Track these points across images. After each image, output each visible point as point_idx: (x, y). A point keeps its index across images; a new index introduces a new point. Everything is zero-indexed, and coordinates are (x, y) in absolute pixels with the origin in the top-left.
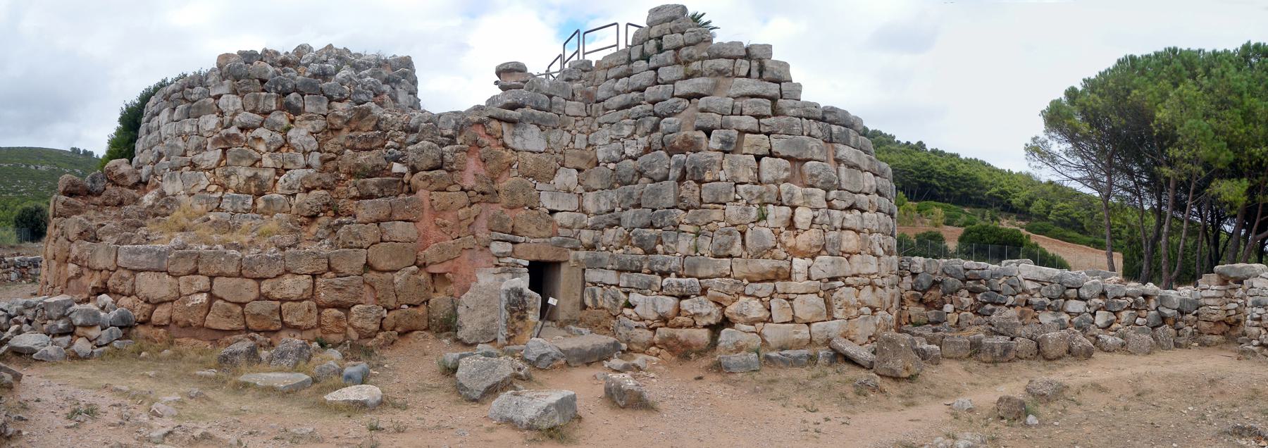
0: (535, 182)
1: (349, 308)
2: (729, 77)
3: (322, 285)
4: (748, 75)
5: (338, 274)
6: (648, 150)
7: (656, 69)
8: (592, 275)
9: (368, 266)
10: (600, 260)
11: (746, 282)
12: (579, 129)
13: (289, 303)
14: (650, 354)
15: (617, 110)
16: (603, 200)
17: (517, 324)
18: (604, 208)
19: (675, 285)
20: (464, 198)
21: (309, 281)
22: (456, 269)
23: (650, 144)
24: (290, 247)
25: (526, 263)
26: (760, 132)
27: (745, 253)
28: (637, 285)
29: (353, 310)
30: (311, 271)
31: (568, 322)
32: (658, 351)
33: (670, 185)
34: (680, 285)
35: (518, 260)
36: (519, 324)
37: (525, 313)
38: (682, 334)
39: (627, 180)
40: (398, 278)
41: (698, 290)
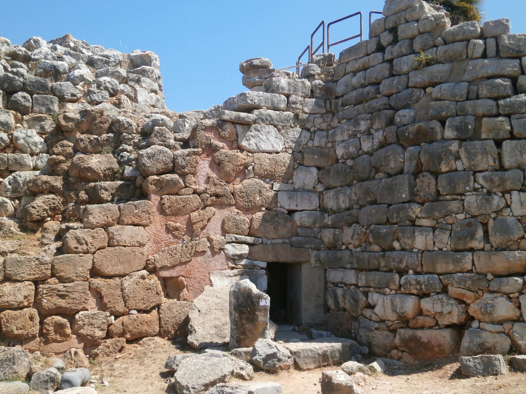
0: (272, 182)
1: (74, 315)
2: (462, 60)
3: (45, 292)
4: (484, 56)
5: (62, 280)
6: (382, 145)
7: (391, 61)
8: (335, 276)
9: (95, 272)
10: (340, 259)
11: (490, 277)
12: (318, 127)
13: (8, 311)
14: (392, 358)
15: (355, 105)
16: (342, 198)
17: (247, 326)
18: (343, 206)
19: (413, 282)
20: (196, 200)
21: (30, 287)
22: (189, 272)
23: (385, 138)
24: (12, 252)
25: (264, 265)
26: (498, 115)
27: (488, 247)
28: (375, 283)
29: (77, 316)
30: (33, 277)
31: (312, 326)
32: (400, 354)
33: (404, 180)
34: (418, 283)
35: (255, 262)
36: (248, 326)
37: (255, 314)
38: (424, 335)
39: (363, 176)
40: (127, 282)
41: (438, 288)
